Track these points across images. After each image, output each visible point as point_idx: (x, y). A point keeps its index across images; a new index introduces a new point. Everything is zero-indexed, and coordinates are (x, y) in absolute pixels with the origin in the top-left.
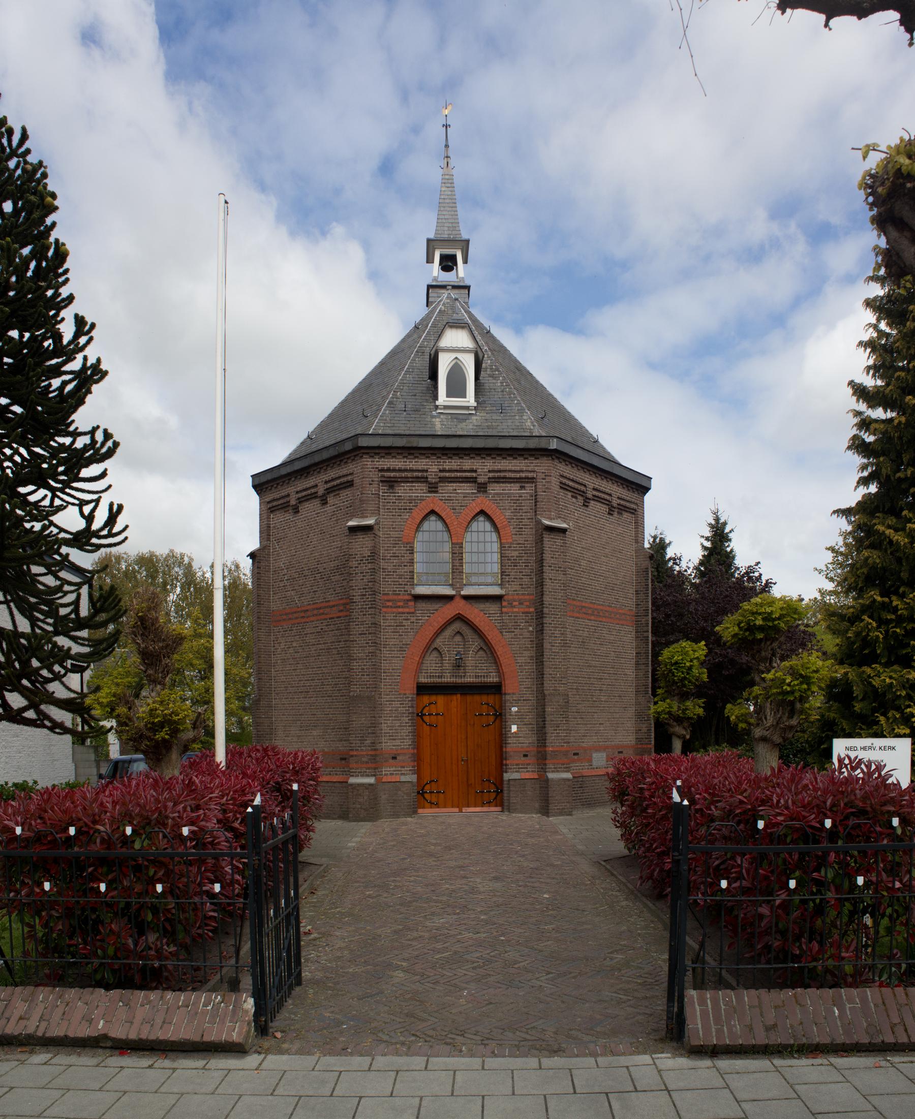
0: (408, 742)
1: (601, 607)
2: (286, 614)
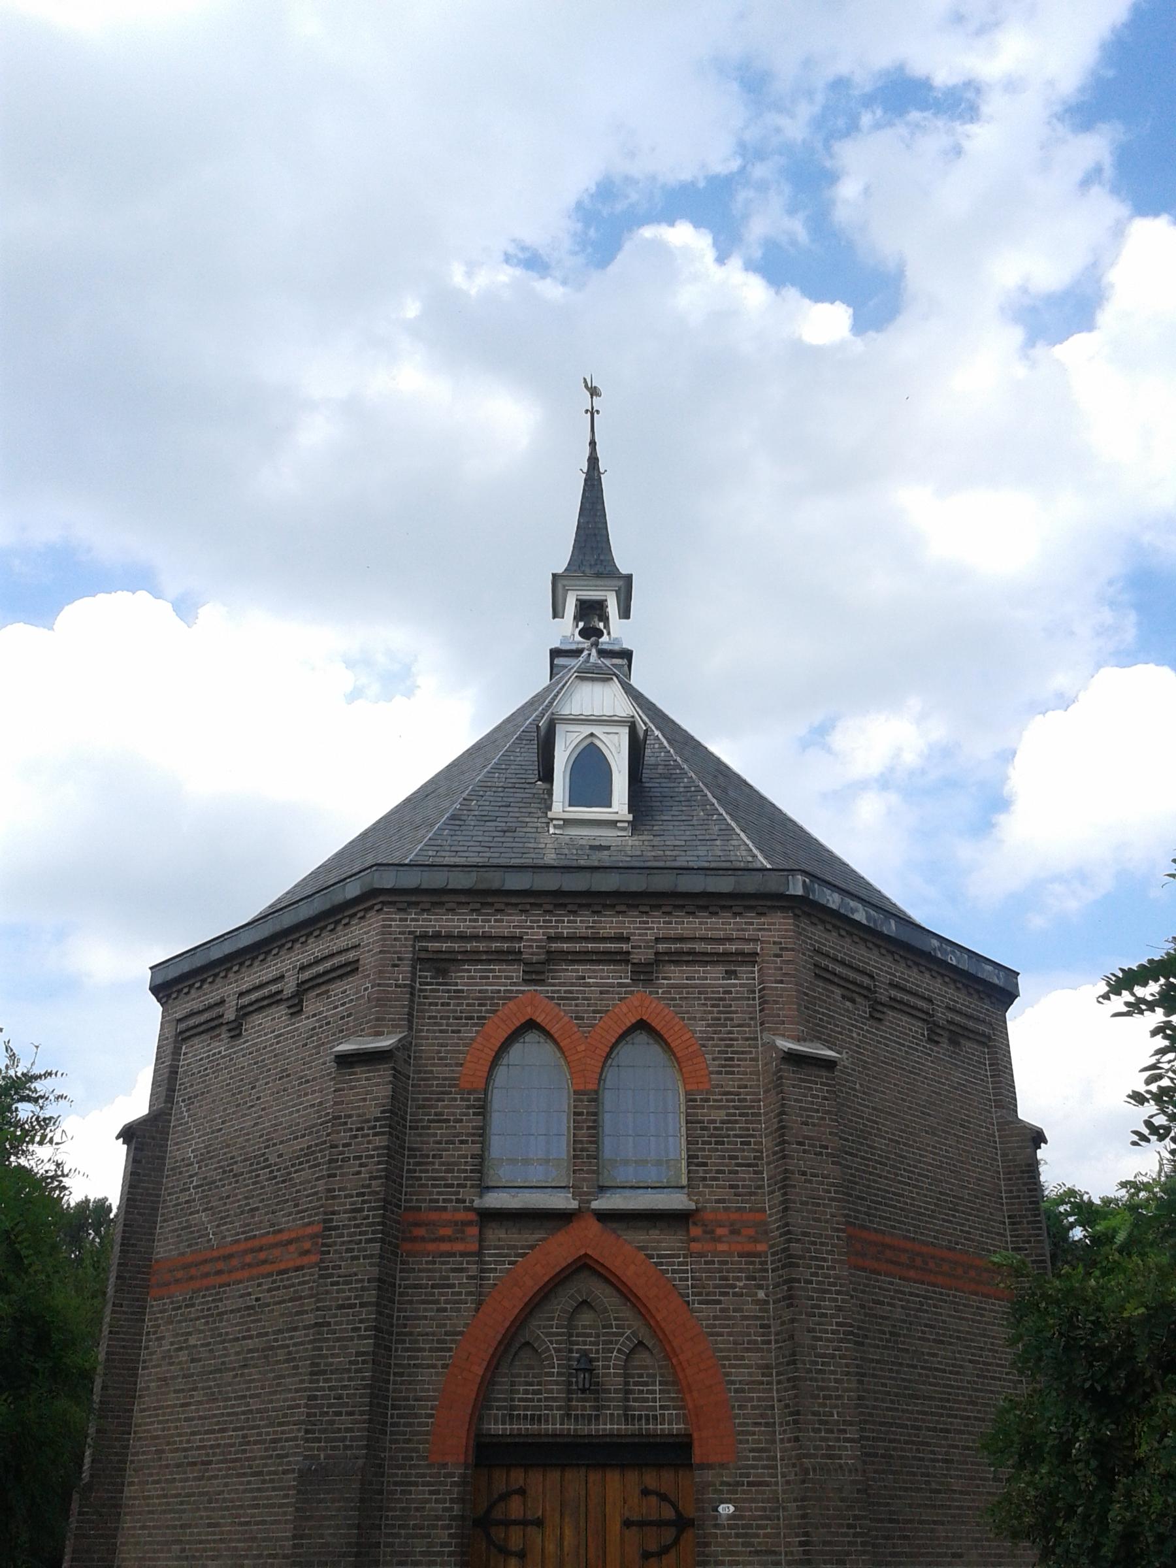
2: (186, 1267)
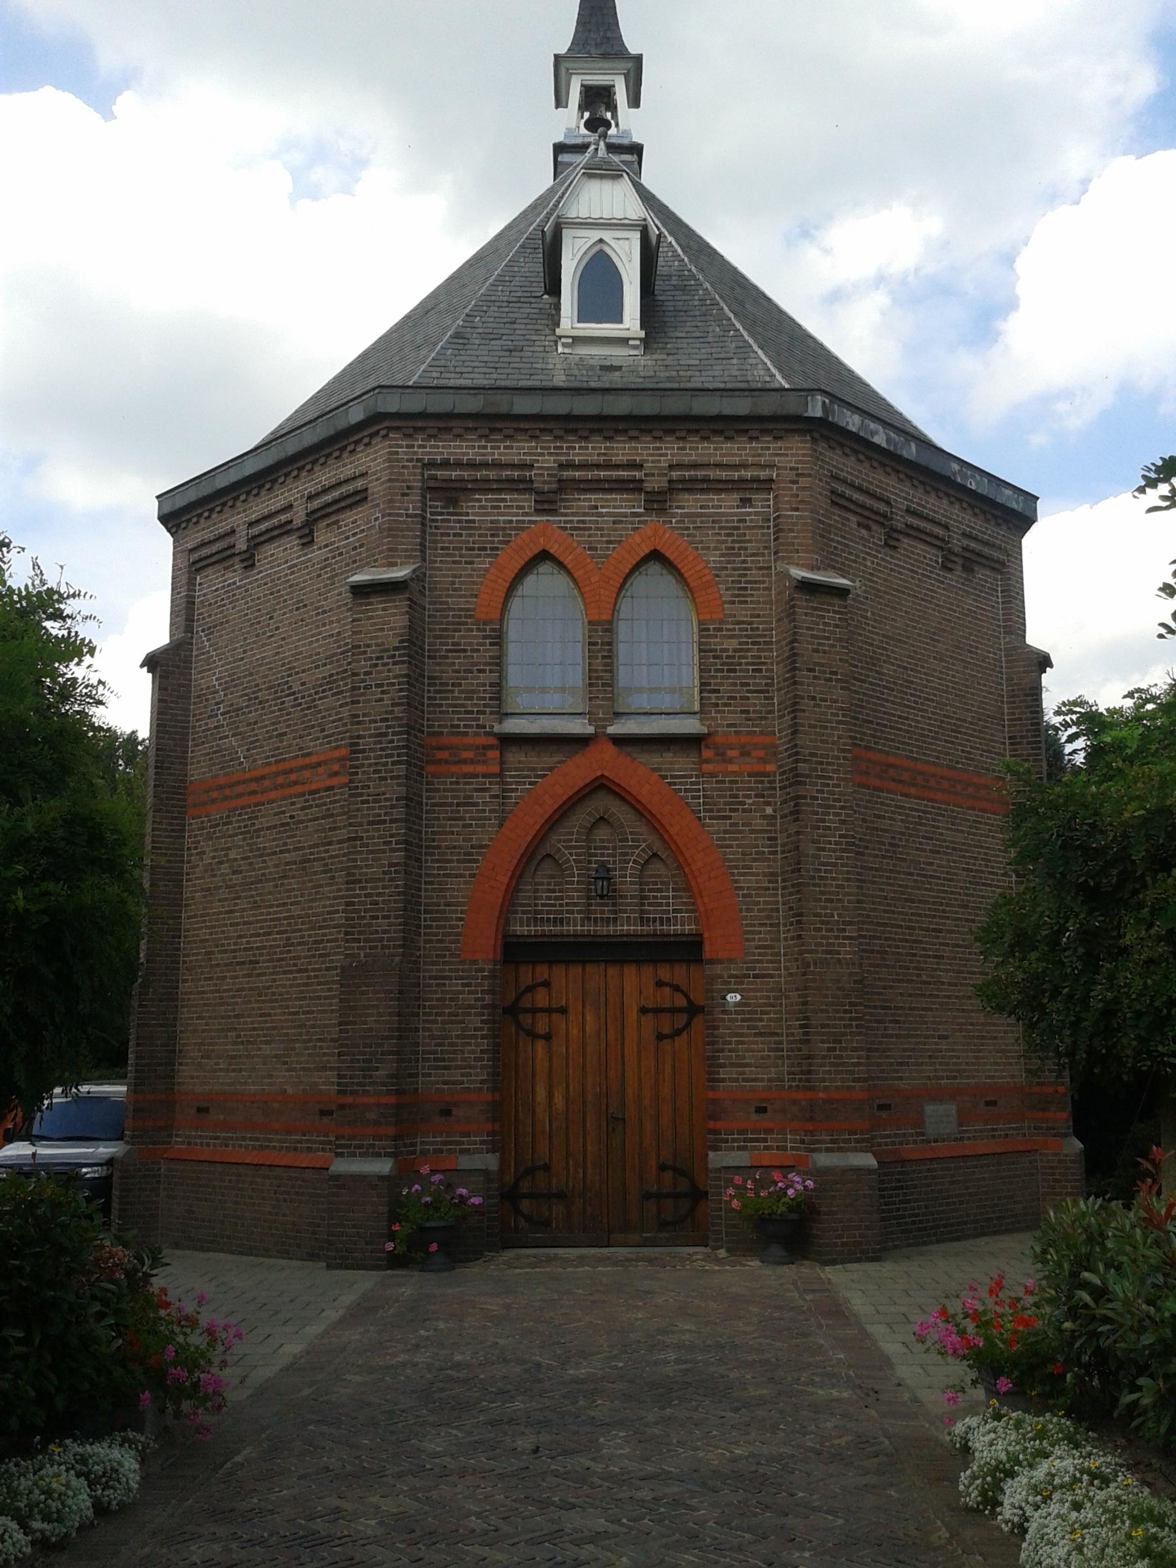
2: (221, 787)
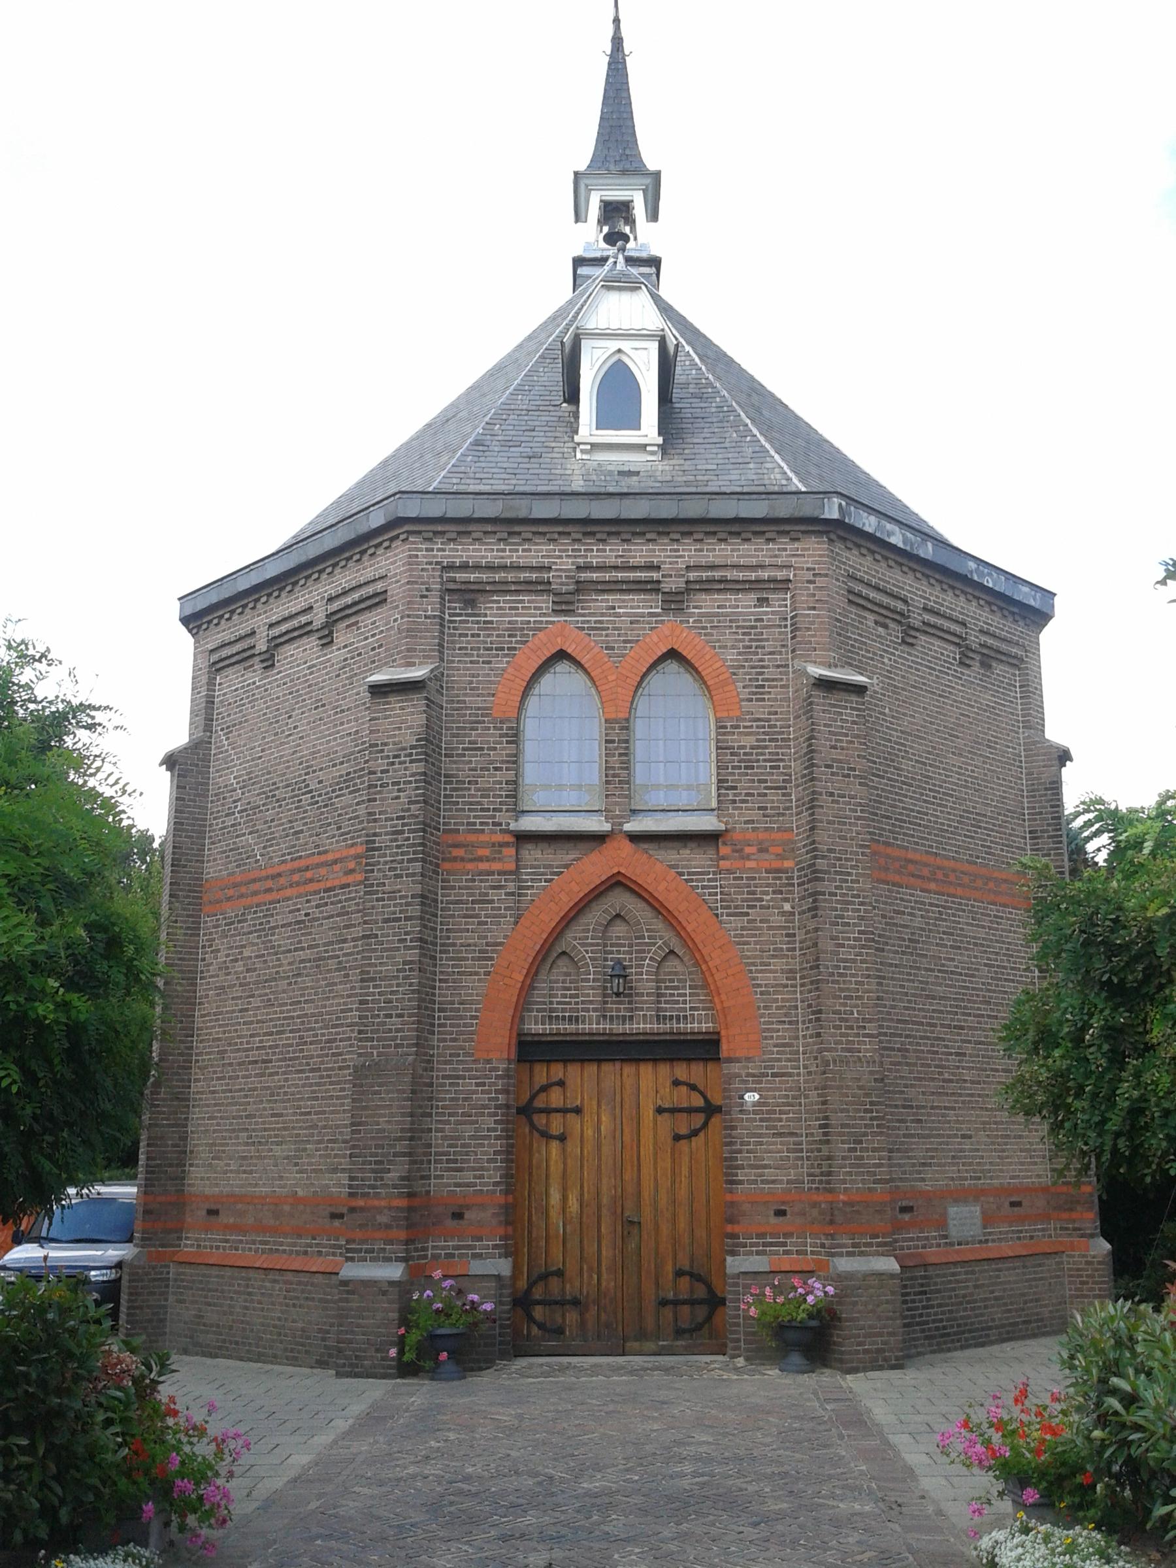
0: (493, 1176)
1: (952, 864)
